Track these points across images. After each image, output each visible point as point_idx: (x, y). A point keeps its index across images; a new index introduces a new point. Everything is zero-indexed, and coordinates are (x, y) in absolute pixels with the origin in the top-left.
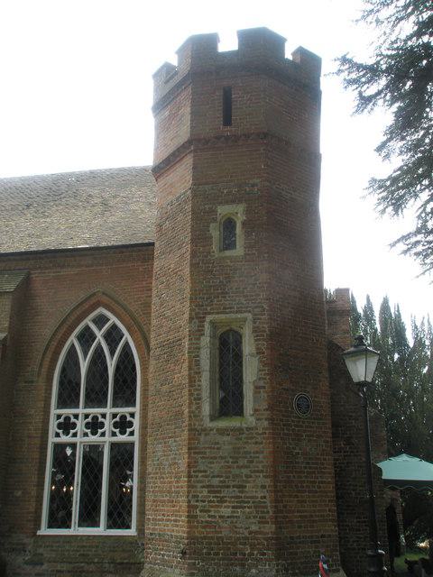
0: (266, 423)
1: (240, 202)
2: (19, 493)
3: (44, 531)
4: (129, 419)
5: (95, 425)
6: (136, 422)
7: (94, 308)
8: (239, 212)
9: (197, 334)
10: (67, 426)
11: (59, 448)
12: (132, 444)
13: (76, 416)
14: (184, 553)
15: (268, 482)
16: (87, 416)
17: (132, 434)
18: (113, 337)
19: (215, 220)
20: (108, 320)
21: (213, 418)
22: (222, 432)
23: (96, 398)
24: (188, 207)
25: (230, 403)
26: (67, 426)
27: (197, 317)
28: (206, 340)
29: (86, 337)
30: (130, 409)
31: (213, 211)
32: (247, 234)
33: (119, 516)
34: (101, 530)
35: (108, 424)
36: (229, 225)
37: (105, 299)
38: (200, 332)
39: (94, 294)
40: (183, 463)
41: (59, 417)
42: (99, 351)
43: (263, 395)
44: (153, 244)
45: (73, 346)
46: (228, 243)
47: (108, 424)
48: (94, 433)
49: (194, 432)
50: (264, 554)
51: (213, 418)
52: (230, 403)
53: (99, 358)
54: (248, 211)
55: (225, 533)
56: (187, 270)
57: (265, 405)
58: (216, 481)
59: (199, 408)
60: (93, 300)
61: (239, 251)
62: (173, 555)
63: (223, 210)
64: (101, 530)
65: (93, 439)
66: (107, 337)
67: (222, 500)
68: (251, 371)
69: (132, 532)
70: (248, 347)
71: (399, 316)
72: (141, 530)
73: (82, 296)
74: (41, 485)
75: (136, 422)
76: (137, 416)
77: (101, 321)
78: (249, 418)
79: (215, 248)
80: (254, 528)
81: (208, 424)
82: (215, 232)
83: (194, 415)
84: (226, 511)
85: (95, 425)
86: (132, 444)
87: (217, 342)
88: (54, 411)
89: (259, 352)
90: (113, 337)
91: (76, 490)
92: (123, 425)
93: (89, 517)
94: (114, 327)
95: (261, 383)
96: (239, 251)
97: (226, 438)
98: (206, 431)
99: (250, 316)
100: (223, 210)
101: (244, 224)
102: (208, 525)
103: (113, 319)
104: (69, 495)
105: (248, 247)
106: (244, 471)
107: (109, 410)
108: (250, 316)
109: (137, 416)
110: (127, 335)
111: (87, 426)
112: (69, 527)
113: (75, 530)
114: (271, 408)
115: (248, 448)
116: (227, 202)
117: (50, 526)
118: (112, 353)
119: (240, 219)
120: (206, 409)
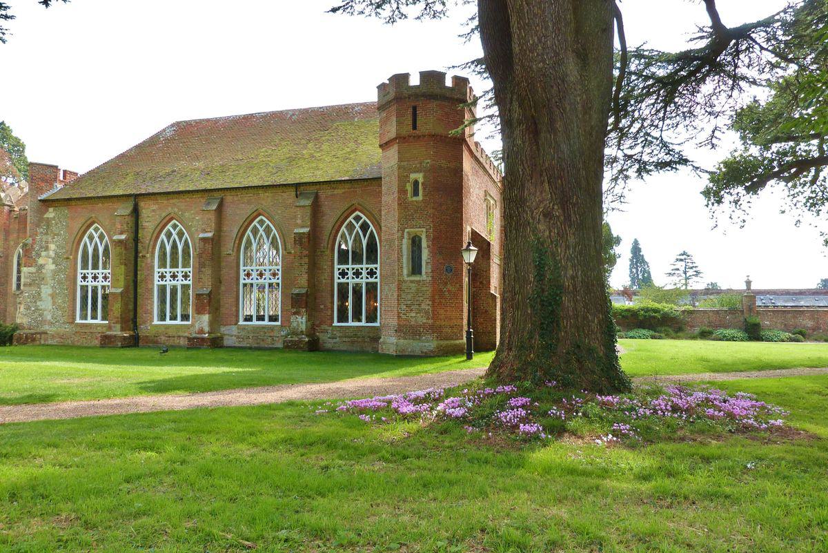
0: (430, 279)
1: (421, 172)
2: (322, 307)
3: (336, 323)
4: (360, 271)
5: (174, 276)
6: (378, 272)
7: (259, 215)
8: (420, 177)
10: (343, 274)
11: (82, 287)
12: (377, 283)
13: (348, 269)
14: (396, 331)
15: (430, 303)
16: (367, 269)
17: (376, 278)
18: (365, 227)
19: (409, 181)
20: (361, 218)
21: (408, 276)
22: (412, 282)
25: (416, 269)
26: (343, 274)
28: (405, 241)
29: (169, 235)
30: (375, 266)
31: (408, 176)
33: (372, 317)
34: (363, 323)
35: (180, 275)
37: (360, 207)
38: (403, 237)
39: (91, 217)
41: (339, 269)
42: (174, 241)
43: (430, 266)
44: (378, 180)
46: (416, 193)
47: (180, 275)
48: (357, 277)
49: (400, 283)
51: (408, 276)
52: (416, 269)
53: (174, 247)
54: (424, 177)
55: (412, 323)
57: (430, 271)
58: (409, 302)
59: (402, 271)
60: (353, 208)
61: (420, 198)
62: (392, 332)
63: (413, 176)
64: (178, 322)
66: (178, 234)
67: (411, 310)
68: (425, 254)
69: (377, 324)
70: (424, 244)
72: (380, 323)
73: (347, 206)
74: (333, 303)
75: (378, 272)
76: (379, 269)
77: (358, 219)
78: (424, 277)
79: (409, 195)
80: (425, 321)
81: (406, 279)
82: (409, 188)
84: (414, 315)
85: (174, 276)
86: (377, 283)
87: (410, 241)
88: (336, 266)
89: (428, 246)
90: (365, 227)
91: (349, 304)
92: (372, 273)
93: (174, 318)
94: (181, 229)
95: (429, 261)
96: (420, 198)
97: (414, 285)
98: (405, 281)
99: (424, 230)
100: (413, 176)
101: (422, 184)
102: (406, 320)
103: (364, 218)
104: (346, 308)
105: (424, 196)
106: (422, 298)
107: (350, 266)
108: (424, 230)
109: (379, 269)
110: (186, 234)
111: (171, 277)
112: (165, 321)
113: (351, 323)
114: (432, 272)
115: (423, 289)
116: (415, 172)
117: (338, 322)
118: (365, 236)
119: (421, 180)
120: (405, 272)
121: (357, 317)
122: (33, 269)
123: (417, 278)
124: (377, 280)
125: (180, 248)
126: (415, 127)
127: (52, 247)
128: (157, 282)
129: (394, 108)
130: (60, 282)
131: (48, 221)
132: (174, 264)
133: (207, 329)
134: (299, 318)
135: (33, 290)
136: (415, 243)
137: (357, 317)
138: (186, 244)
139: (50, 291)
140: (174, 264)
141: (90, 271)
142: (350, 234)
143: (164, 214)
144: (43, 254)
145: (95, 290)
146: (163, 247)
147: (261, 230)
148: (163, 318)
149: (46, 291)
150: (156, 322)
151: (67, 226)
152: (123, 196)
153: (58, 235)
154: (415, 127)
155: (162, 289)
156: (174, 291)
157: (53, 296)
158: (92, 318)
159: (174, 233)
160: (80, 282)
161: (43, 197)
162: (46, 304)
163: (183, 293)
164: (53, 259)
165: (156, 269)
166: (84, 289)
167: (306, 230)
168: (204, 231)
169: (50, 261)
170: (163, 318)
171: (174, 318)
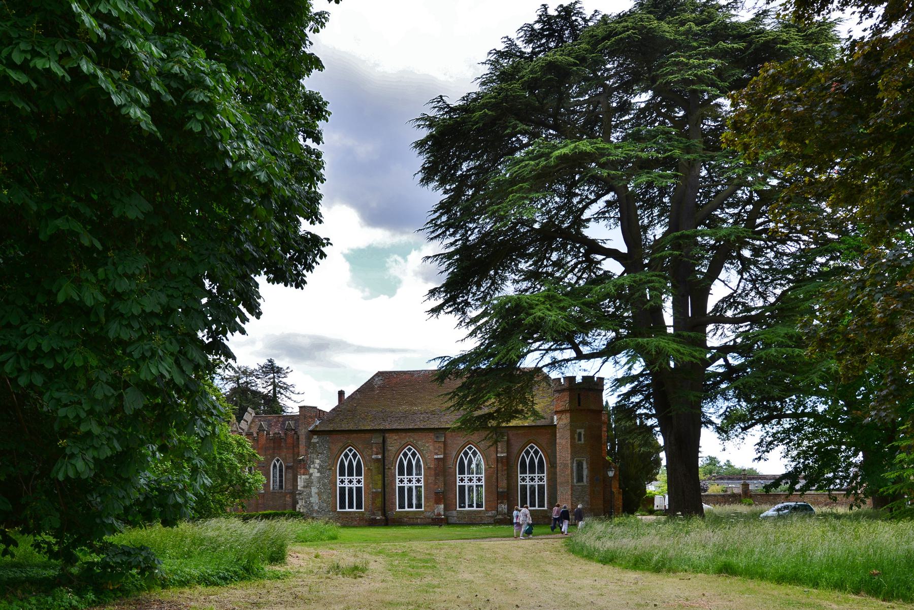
8: (582, 431)
9: (572, 463)
23: (532, 471)
24: (568, 427)
25: (580, 479)
27: (572, 459)
28: (575, 465)
29: (405, 455)
32: (585, 438)
34: (354, 510)
35: (536, 479)
36: (580, 434)
40: (569, 493)
45: (523, 456)
46: (580, 439)
47: (536, 479)
49: (573, 486)
50: (745, 557)
52: (580, 479)
56: (569, 447)
63: (578, 431)
65: (532, 483)
66: (412, 454)
70: (585, 466)
71: (352, 250)
82: (576, 436)
83: (572, 482)
94: (536, 449)
100: (578, 431)
104: (416, 469)
113: (347, 510)
119: (583, 433)
120: (575, 481)
121: (351, 506)
122: (307, 477)
123: (582, 484)
124: (362, 485)
125: (355, 464)
126: (579, 405)
127: (318, 461)
128: (398, 484)
129: (568, 393)
130: (324, 485)
131: (315, 444)
132: (350, 474)
133: (442, 513)
134: (503, 506)
135: (307, 490)
136: (580, 465)
137: (471, 506)
138: (418, 460)
139: (316, 491)
140: (350, 474)
141: (355, 477)
142: (475, 456)
143: (403, 442)
144: (312, 466)
145: (410, 489)
146: (401, 462)
147: (470, 453)
148: (402, 506)
149: (314, 490)
150: (398, 510)
151: (329, 448)
152: (370, 430)
153: (321, 454)
154: (579, 405)
155: (462, 488)
156: (410, 489)
157: (319, 494)
158: (349, 508)
159: (409, 454)
160: (339, 485)
161: (310, 428)
162: (314, 499)
163: (477, 490)
164: (318, 469)
165: (397, 477)
166: (342, 490)
167: (505, 455)
168: (437, 454)
169: (316, 470)
170: (402, 506)
171: (410, 506)
